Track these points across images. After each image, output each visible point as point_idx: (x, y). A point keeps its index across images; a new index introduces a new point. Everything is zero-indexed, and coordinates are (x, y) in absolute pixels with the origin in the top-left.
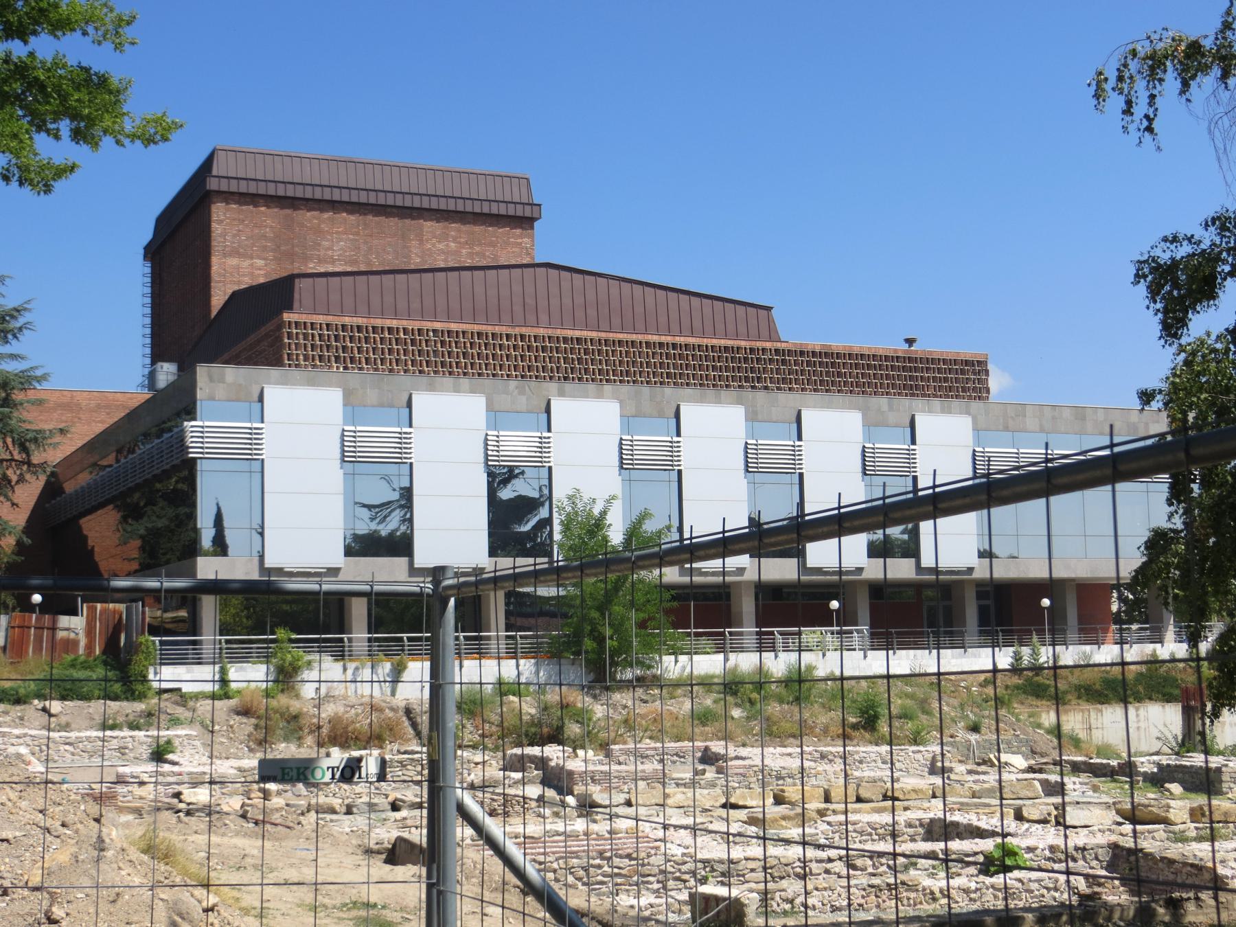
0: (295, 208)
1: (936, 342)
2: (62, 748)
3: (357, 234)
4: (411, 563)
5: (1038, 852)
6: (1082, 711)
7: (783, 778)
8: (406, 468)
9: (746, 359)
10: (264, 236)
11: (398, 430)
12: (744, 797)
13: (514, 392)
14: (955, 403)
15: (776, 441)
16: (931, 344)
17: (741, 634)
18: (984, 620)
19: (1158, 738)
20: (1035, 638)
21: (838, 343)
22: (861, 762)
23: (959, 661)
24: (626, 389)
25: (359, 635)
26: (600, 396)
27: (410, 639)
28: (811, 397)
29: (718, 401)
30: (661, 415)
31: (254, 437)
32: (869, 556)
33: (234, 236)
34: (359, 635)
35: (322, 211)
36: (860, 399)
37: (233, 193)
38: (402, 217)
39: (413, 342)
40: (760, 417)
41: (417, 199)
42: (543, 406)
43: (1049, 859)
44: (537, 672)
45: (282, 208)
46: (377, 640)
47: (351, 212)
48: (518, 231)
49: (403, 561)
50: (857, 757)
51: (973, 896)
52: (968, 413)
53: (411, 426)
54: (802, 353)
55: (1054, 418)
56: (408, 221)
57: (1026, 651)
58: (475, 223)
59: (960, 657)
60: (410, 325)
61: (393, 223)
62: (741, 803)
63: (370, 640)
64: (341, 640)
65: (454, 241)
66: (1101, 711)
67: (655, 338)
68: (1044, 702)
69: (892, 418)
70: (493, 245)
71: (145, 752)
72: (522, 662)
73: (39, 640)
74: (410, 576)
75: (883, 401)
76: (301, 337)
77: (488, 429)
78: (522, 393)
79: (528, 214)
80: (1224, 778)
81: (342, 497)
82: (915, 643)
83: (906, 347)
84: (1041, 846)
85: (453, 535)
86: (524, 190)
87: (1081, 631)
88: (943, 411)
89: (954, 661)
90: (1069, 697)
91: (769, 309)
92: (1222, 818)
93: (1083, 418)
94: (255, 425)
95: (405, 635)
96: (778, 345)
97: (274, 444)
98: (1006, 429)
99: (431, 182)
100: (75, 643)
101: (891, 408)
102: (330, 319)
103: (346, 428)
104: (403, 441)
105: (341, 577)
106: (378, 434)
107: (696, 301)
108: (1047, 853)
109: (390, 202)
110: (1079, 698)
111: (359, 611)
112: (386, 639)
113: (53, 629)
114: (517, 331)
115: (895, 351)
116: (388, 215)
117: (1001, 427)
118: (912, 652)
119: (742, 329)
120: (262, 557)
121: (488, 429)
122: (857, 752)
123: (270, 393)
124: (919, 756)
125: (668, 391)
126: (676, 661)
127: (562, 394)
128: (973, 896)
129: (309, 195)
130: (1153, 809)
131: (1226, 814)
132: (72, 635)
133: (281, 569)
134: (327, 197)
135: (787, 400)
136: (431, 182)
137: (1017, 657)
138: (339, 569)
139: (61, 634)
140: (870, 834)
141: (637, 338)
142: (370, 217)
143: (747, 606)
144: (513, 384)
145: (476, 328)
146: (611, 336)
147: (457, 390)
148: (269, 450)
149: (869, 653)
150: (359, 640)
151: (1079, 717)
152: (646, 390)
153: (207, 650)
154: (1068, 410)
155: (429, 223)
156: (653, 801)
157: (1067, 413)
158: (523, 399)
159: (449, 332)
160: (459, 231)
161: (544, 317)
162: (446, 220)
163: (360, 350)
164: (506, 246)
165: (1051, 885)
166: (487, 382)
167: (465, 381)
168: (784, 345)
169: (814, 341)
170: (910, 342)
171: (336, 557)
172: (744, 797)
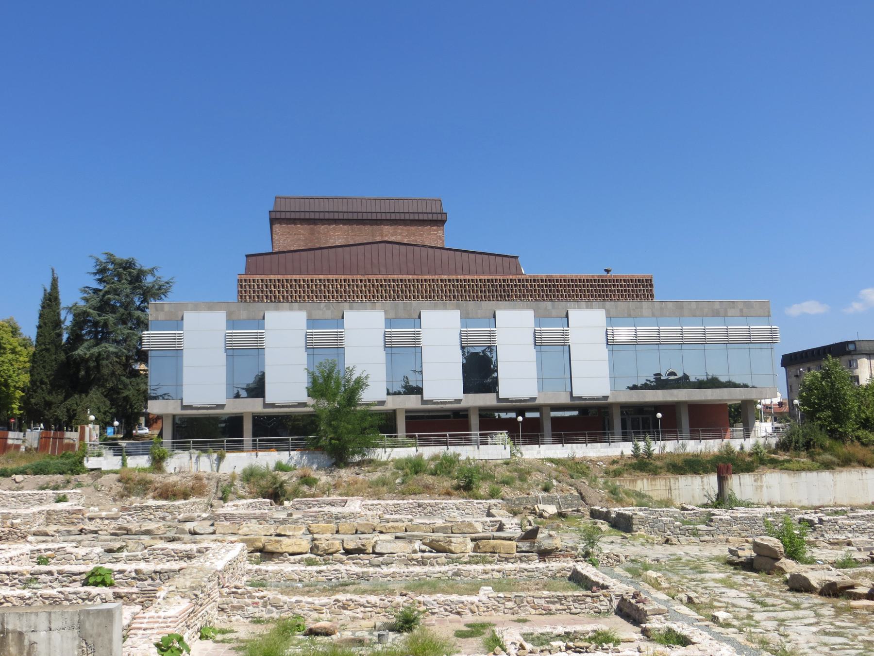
0: (316, 224)
1: (625, 269)
2: (11, 499)
4: (422, 397)
5: (126, 573)
8: (566, 348)
12: (285, 530)
13: (324, 310)
14: (595, 303)
15: (552, 330)
16: (618, 272)
20: (648, 438)
21: (556, 274)
22: (443, 509)
23: (605, 450)
24: (389, 304)
26: (374, 308)
27: (450, 435)
28: (571, 303)
29: (445, 308)
30: (410, 317)
35: (329, 224)
36: (534, 303)
38: (405, 225)
41: (379, 215)
42: (565, 314)
43: (134, 578)
44: (301, 458)
47: (344, 224)
48: (435, 228)
49: (495, 394)
51: (27, 601)
52: (604, 308)
54: (535, 280)
55: (661, 308)
57: (642, 444)
58: (411, 225)
59: (606, 447)
60: (306, 277)
61: (367, 227)
63: (173, 443)
65: (400, 234)
69: (554, 313)
70: (421, 235)
72: (292, 453)
73: (54, 444)
75: (548, 304)
81: (225, 368)
82: (577, 440)
84: (129, 570)
85: (444, 385)
86: (438, 206)
87: (691, 432)
88: (587, 308)
89: (602, 450)
90: (662, 470)
91: (517, 257)
92: (492, 550)
93: (681, 308)
95: (290, 438)
96: (520, 277)
98: (630, 316)
99: (434, 207)
100: (73, 446)
101: (553, 307)
104: (565, 334)
108: (133, 574)
110: (668, 471)
111: (248, 426)
113: (62, 438)
116: (364, 224)
118: (574, 445)
119: (500, 269)
120: (571, 393)
124: (480, 506)
125: (414, 304)
127: (351, 308)
128: (27, 601)
130: (442, 544)
131: (493, 547)
132: (72, 442)
135: (487, 306)
136: (434, 207)
137: (637, 448)
139: (66, 441)
140: (173, 556)
141: (435, 277)
143: (474, 420)
144: (323, 305)
147: (291, 309)
148: (424, 342)
150: (248, 441)
151: (663, 482)
152: (401, 304)
155: (386, 227)
156: (230, 531)
157: (670, 305)
161: (383, 269)
162: (396, 224)
164: (429, 236)
165: (84, 597)
166: (309, 304)
167: (296, 305)
168: (523, 277)
169: (542, 274)
170: (608, 271)
171: (303, 397)
172: (285, 530)
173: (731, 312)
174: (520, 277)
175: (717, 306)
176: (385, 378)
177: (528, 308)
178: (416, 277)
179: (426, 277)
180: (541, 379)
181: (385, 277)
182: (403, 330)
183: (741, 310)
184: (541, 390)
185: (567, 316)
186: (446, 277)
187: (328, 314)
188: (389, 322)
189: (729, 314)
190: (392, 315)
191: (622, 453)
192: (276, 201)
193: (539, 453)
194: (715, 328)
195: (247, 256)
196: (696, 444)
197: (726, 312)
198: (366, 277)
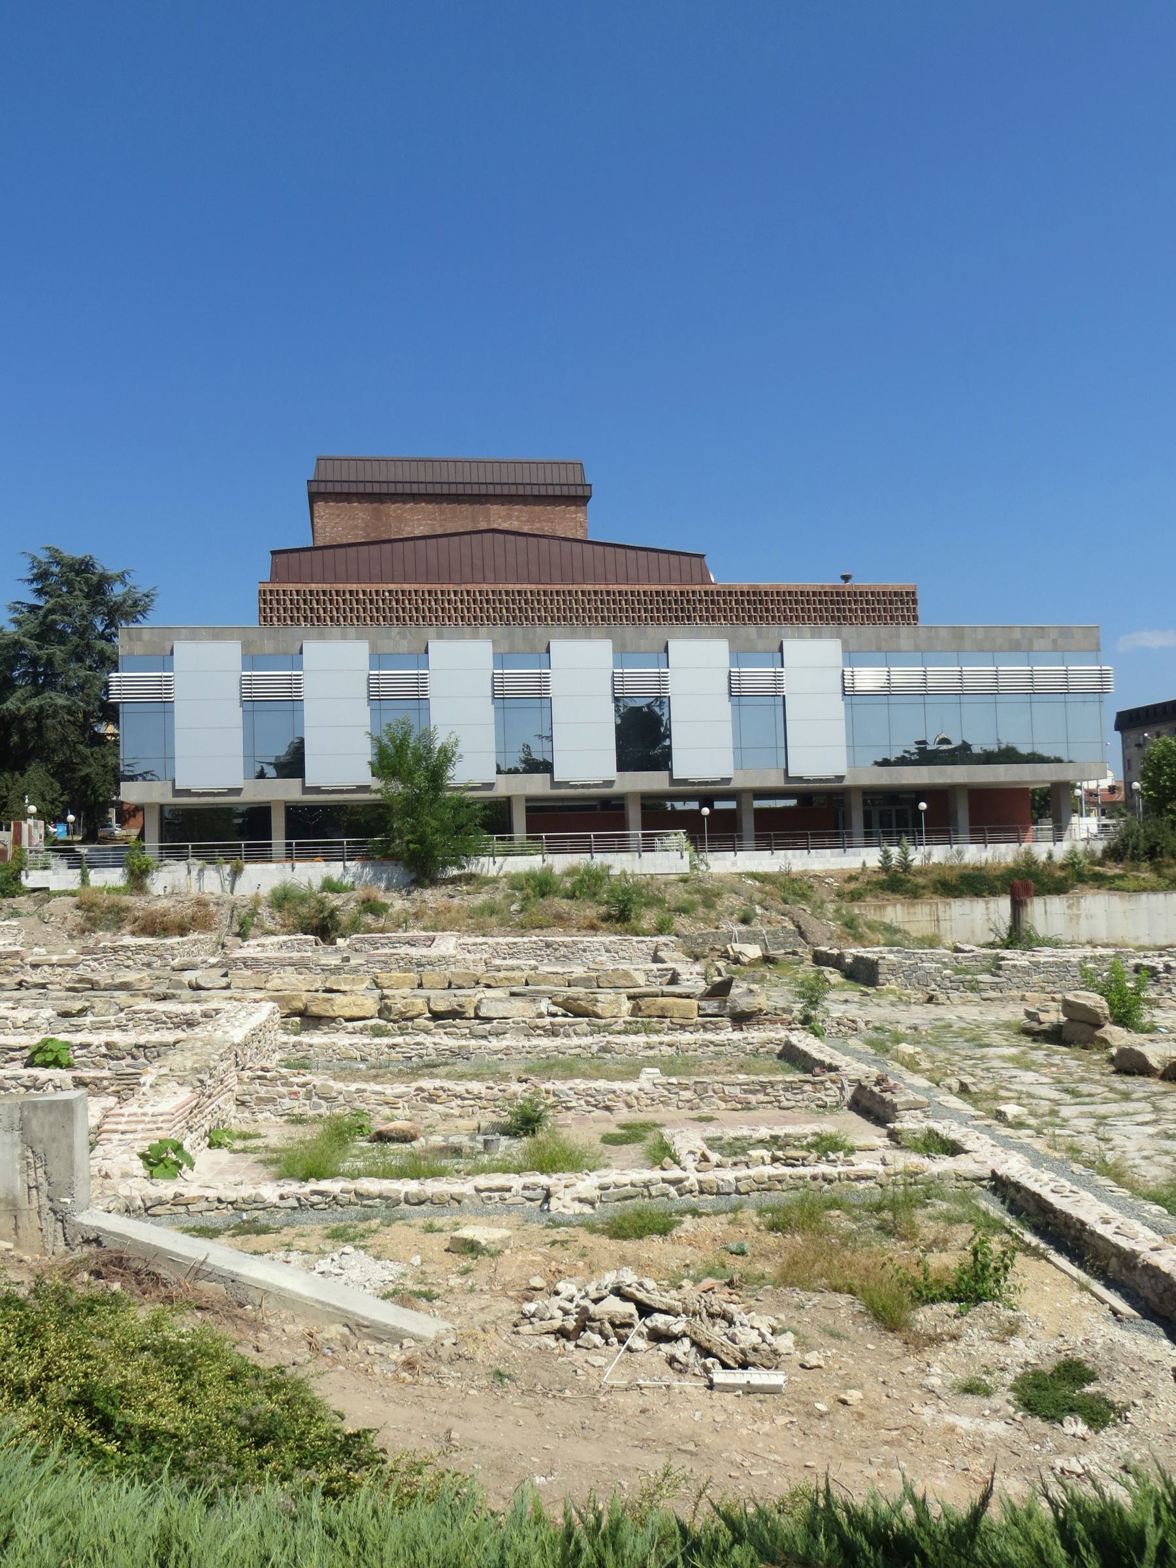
0: (382, 502)
3: (434, 519)
6: (930, 904)
7: (422, 965)
8: (779, 700)
9: (700, 601)
10: (356, 527)
12: (338, 982)
13: (396, 639)
14: (826, 629)
15: (757, 674)
17: (1042, 830)
18: (868, 823)
19: (991, 930)
21: (764, 584)
23: (838, 859)
24: (500, 630)
25: (278, 841)
26: (475, 637)
29: (588, 636)
30: (533, 651)
31: (543, 680)
32: (619, 770)
33: (333, 528)
34: (278, 841)
35: (404, 502)
37: (330, 494)
39: (713, 602)
40: (628, 649)
42: (777, 648)
43: (104, 1056)
45: (371, 503)
47: (428, 502)
48: (573, 508)
50: (581, 946)
56: (476, 507)
57: (895, 851)
59: (840, 855)
62: (335, 988)
63: (161, 848)
65: (518, 519)
66: (949, 904)
67: (616, 588)
68: (898, 896)
69: (760, 645)
71: (755, 921)
75: (751, 630)
76: (274, 602)
79: (580, 493)
80: (880, 970)
83: (842, 583)
84: (96, 1043)
85: (586, 757)
86: (578, 473)
92: (659, 1013)
95: (544, 835)
96: (707, 587)
97: (793, 682)
98: (879, 650)
99: (570, 474)
101: (759, 636)
102: (299, 586)
104: (777, 679)
106: (757, 674)
107: (631, 553)
108: (103, 1050)
109: (461, 491)
110: (935, 893)
111: (278, 823)
114: (463, 587)
115: (823, 587)
120: (786, 771)
121: (371, 669)
122: (582, 942)
123: (555, 645)
124: (643, 946)
125: (540, 630)
126: (495, 862)
127: (440, 637)
129: (392, 491)
131: (662, 1009)
133: (189, 790)
134: (408, 491)
135: (654, 633)
136: (570, 474)
137: (887, 857)
138: (730, 779)
140: (165, 1023)
142: (445, 505)
143: (634, 814)
144: (395, 631)
145: (427, 587)
146: (549, 587)
148: (554, 690)
149: (643, 854)
151: (927, 909)
152: (519, 630)
153: (633, 842)
155: (495, 507)
156: (253, 985)
157: (943, 633)
158: (405, 642)
159: (403, 592)
160: (521, 511)
163: (755, 610)
164: (562, 522)
167: (352, 631)
169: (743, 583)
170: (846, 578)
171: (365, 777)
173: (1038, 644)
175: (1017, 635)
178: (542, 587)
180: (739, 749)
181: (493, 587)
183: (1054, 642)
184: (739, 765)
185: (781, 650)
187: (403, 646)
188: (500, 660)
192: (318, 465)
194: (1013, 670)
195: (273, 553)
196: (979, 850)
197: (1030, 641)
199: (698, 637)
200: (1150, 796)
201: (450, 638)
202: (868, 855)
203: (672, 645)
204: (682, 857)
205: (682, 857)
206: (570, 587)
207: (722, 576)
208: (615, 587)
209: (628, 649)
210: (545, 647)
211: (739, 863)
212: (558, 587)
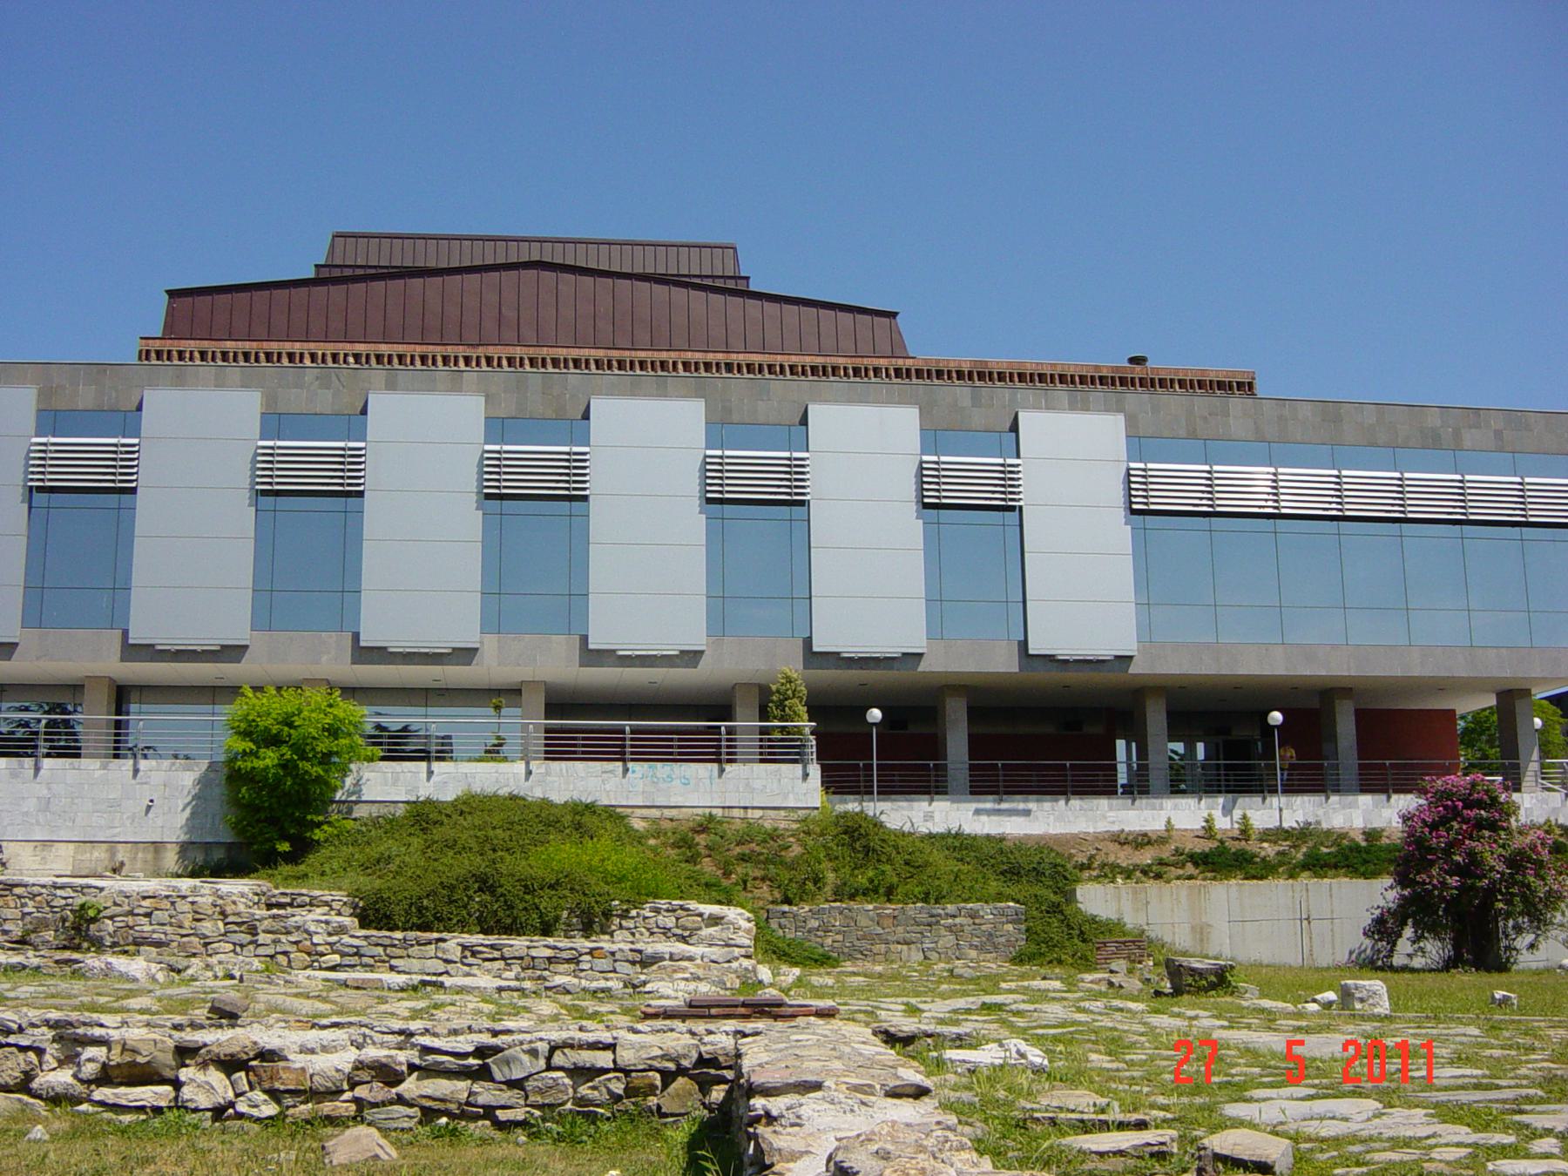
11: (1000, 461)
13: (310, 390)
15: (970, 467)
26: (456, 387)
46: (893, 767)
53: (1018, 456)
64: (1321, 767)
69: (978, 418)
74: (356, 660)
77: (1130, 460)
78: (326, 385)
86: (730, 263)
88: (1073, 407)
91: (894, 315)
94: (1009, 461)
95: (1000, 763)
96: (900, 362)
98: (1192, 435)
99: (718, 262)
101: (976, 402)
103: (1132, 465)
104: (1008, 476)
105: (704, 662)
112: (1025, 767)
117: (1182, 433)
119: (847, 344)
120: (1024, 644)
121: (1130, 460)
127: (391, 386)
136: (718, 262)
138: (698, 654)
147: (220, 384)
148: (1028, 495)
154: (1309, 406)
157: (1305, 411)
158: (328, 395)
168: (909, 362)
173: (1469, 438)
174: (900, 362)
175: (1433, 420)
176: (476, 582)
177: (902, 401)
178: (615, 354)
179: (642, 355)
180: (936, 600)
181: (532, 352)
182: (538, 451)
183: (1498, 434)
184: (935, 630)
185: (1014, 428)
186: (699, 356)
187: (324, 401)
188: (497, 428)
189: (1467, 444)
190: (506, 408)
191: (1169, 822)
192: (332, 246)
193: (929, 817)
194: (1430, 485)
195: (172, 294)
196: (1376, 805)
197: (1457, 434)
198: (481, 351)
199: (862, 400)
200: (1481, 877)
201: (409, 389)
202: (1175, 807)
203: (815, 411)
204: (806, 776)
205: (806, 776)
206: (664, 356)
207: (922, 348)
208: (741, 356)
209: (735, 418)
210: (583, 408)
211: (937, 816)
212: (642, 355)
